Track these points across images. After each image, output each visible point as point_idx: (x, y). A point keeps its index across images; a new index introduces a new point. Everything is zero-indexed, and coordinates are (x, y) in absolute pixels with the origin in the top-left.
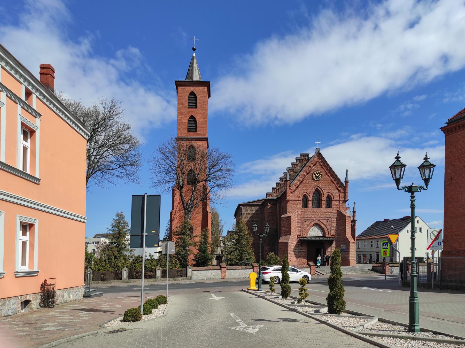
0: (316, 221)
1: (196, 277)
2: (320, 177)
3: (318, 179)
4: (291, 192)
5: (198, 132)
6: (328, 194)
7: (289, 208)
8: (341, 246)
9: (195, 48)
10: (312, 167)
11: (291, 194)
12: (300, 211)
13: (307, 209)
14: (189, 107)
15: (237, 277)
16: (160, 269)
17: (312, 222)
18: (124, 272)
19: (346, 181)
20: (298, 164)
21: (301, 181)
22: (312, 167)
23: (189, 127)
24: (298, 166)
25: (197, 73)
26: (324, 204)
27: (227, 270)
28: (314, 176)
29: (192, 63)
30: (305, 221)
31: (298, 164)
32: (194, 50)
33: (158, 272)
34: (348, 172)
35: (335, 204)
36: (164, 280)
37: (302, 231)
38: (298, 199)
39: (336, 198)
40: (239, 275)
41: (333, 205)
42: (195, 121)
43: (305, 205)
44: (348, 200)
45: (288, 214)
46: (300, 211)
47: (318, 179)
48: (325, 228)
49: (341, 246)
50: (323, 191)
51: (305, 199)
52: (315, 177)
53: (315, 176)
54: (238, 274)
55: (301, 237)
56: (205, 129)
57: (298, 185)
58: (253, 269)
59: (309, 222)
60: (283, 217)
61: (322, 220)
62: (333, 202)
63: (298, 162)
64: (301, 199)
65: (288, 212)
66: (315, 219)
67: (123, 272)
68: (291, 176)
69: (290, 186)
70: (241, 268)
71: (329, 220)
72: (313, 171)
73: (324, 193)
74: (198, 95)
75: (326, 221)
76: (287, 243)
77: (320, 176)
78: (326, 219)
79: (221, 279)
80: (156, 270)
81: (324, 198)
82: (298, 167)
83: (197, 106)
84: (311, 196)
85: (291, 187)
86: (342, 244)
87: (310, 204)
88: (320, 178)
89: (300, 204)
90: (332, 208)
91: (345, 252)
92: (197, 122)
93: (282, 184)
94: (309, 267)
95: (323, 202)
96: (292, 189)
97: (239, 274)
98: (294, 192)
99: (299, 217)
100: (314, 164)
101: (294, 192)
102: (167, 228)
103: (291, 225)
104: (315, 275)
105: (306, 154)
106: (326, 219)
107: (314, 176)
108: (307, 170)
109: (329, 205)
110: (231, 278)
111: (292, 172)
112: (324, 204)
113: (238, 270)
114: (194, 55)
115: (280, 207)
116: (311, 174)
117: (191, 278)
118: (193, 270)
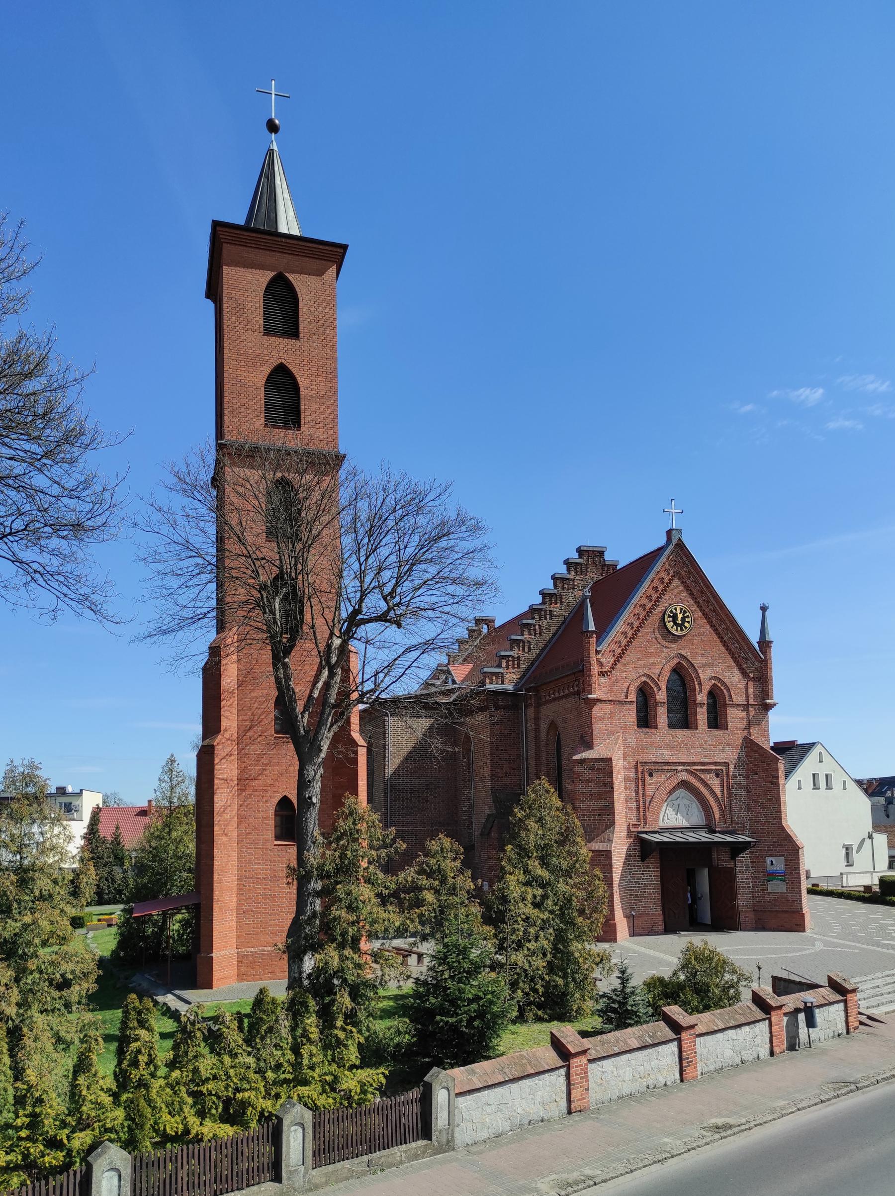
0: (684, 776)
1: (469, 1125)
2: (686, 624)
3: (682, 630)
4: (602, 674)
5: (305, 429)
6: (645, 682)
7: (598, 728)
8: (768, 862)
9: (277, 122)
10: (660, 589)
11: (602, 679)
12: (632, 739)
13: (653, 730)
14: (268, 331)
15: (626, 1090)
16: (302, 1117)
17: (672, 779)
18: (105, 1184)
19: (765, 644)
20: (573, 580)
21: (630, 635)
22: (660, 589)
23: (269, 407)
24: (574, 584)
25: (291, 213)
26: (702, 715)
27: (591, 1067)
28: (669, 622)
29: (267, 175)
30: (651, 775)
31: (573, 580)
32: (271, 132)
33: (295, 1140)
34: (767, 613)
35: (735, 717)
36: (327, 1182)
37: (643, 807)
38: (622, 697)
39: (738, 696)
40: (634, 1080)
41: (729, 719)
42: (294, 388)
43: (645, 720)
44: (775, 705)
45: (596, 747)
46: (632, 739)
47: (683, 633)
48: (711, 800)
49: (768, 862)
50: (700, 671)
51: (645, 695)
52: (672, 624)
53: (671, 619)
54: (628, 1074)
55: (639, 829)
56: (332, 422)
57: (622, 650)
58: (679, 1041)
59: (663, 776)
60: (582, 761)
61: (700, 770)
62: (730, 711)
63: (573, 573)
64: (633, 697)
65: (595, 742)
66: (680, 768)
67: (100, 1181)
68: (556, 616)
69: (597, 652)
70: (635, 1044)
71: (722, 770)
72: (664, 603)
73: (702, 677)
74: (303, 292)
75: (713, 775)
76: (610, 852)
77: (688, 622)
78: (713, 767)
79: (570, 1112)
80: (285, 1128)
81: (702, 698)
82: (574, 589)
83: (301, 330)
84: (663, 686)
85: (599, 656)
86: (771, 855)
87: (662, 715)
88: (686, 627)
89: (630, 715)
90: (696, 728)
91: (784, 881)
92: (302, 391)
93: (528, 641)
94: (841, 998)
95: (699, 709)
96: (603, 661)
97: (631, 1077)
98: (611, 672)
99: (630, 759)
100: (666, 580)
101: (611, 672)
102: (158, 793)
103: (613, 788)
104: (861, 1027)
105: (591, 549)
106: (713, 767)
107: (669, 622)
108: (645, 601)
109: (716, 721)
110: (606, 1098)
111: (558, 605)
112: (702, 715)
113: (628, 1055)
114: (275, 147)
115: (537, 719)
116: (658, 612)
117: (448, 1142)
118: (459, 1095)
